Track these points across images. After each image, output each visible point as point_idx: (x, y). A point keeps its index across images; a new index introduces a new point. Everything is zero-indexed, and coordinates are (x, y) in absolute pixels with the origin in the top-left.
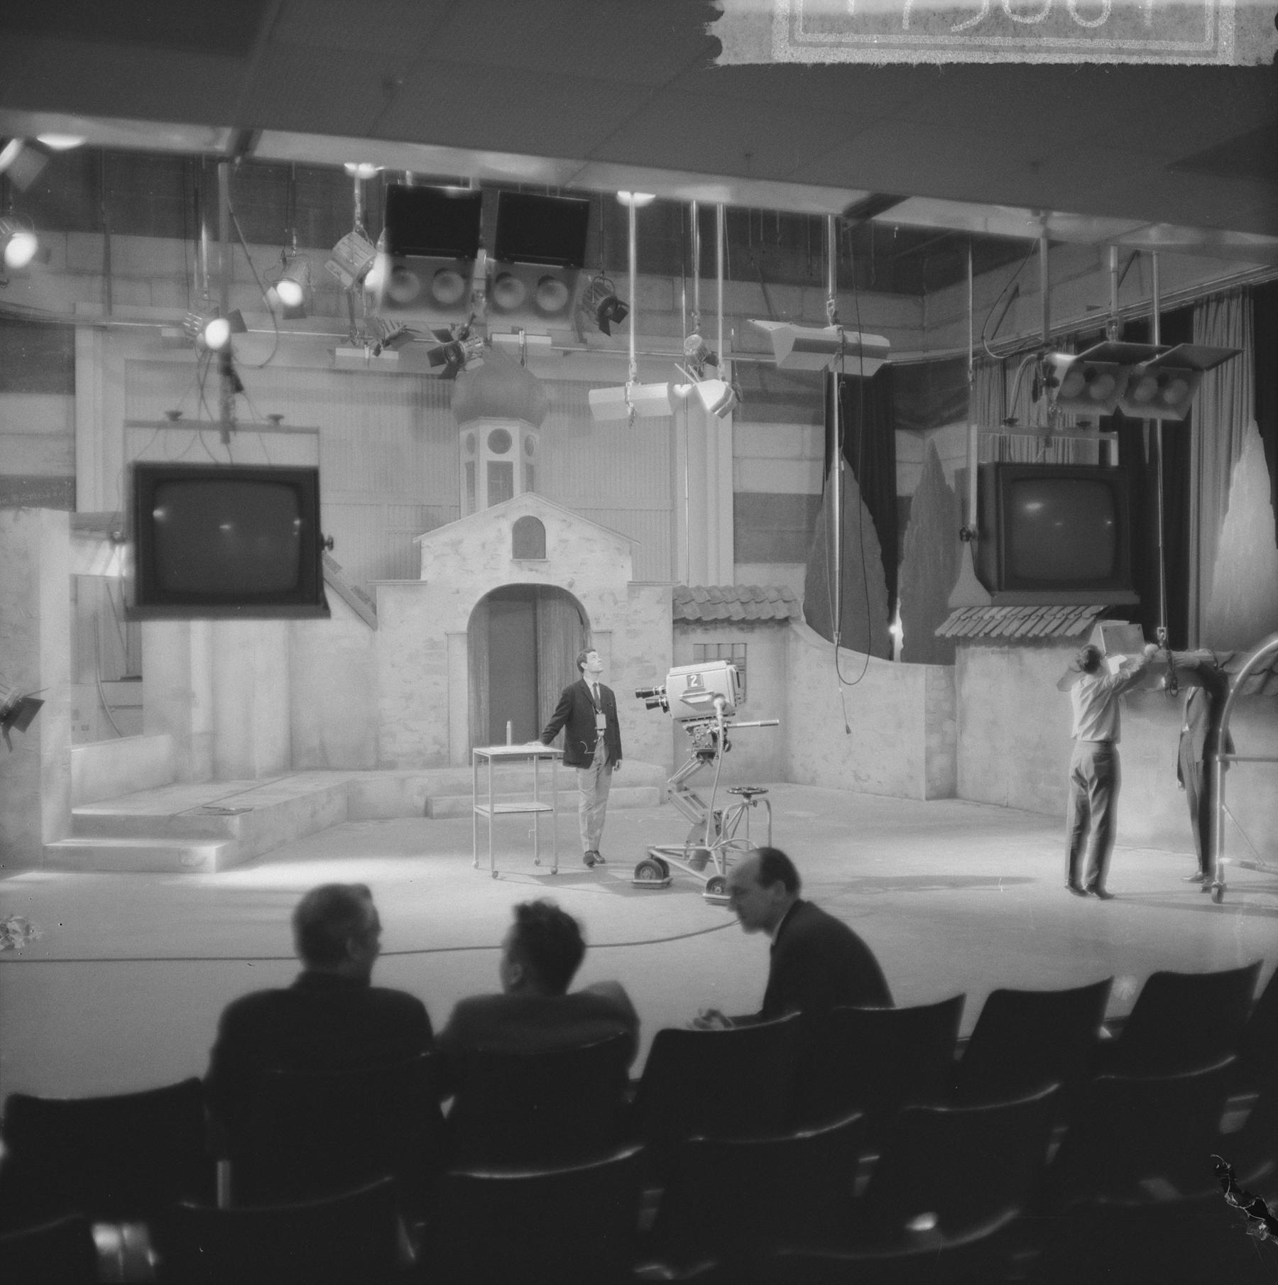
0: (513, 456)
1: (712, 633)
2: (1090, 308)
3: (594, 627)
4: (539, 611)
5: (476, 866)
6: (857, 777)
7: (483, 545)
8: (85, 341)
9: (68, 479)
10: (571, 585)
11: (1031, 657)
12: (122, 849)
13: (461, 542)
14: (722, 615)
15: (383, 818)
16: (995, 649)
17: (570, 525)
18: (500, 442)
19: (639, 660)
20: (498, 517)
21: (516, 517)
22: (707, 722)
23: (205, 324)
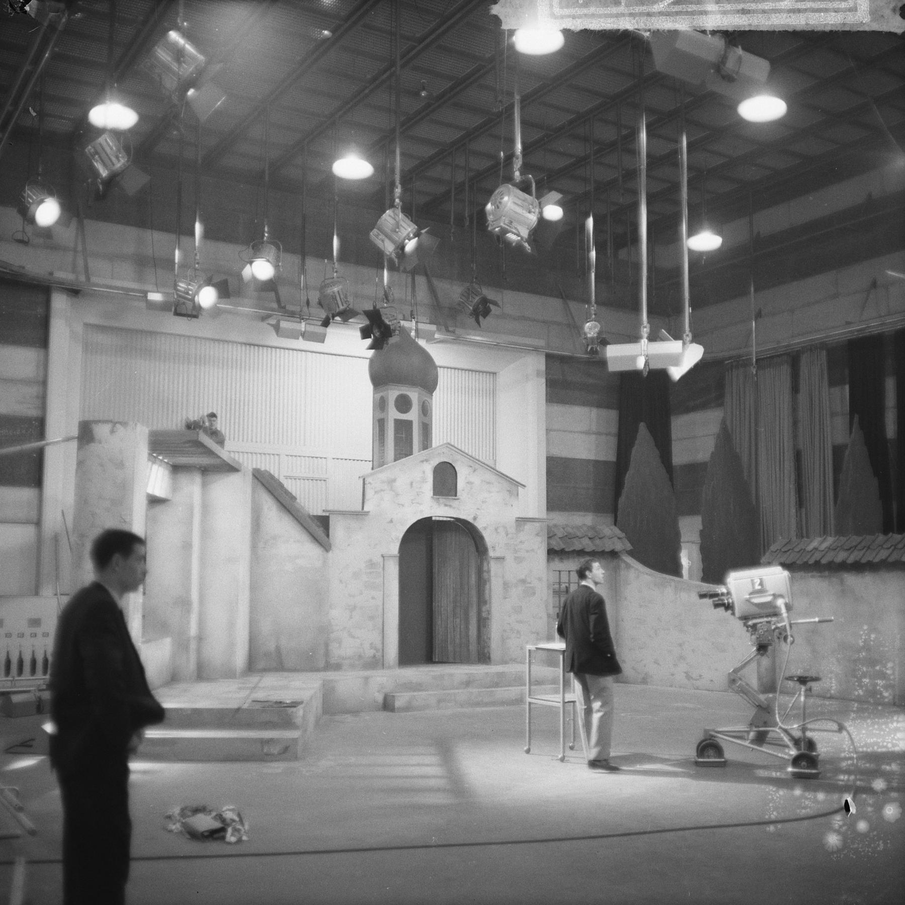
0: (413, 415)
1: (565, 562)
2: (848, 323)
3: (491, 553)
4: (436, 541)
5: (528, 751)
6: (688, 677)
7: (412, 484)
8: (59, 302)
9: (36, 419)
10: (475, 519)
11: (852, 580)
12: (214, 739)
13: (394, 480)
14: (578, 546)
15: (355, 712)
16: (815, 573)
17: (475, 471)
18: (403, 404)
19: (523, 581)
20: (422, 461)
21: (435, 462)
22: (769, 619)
23: (276, 267)
